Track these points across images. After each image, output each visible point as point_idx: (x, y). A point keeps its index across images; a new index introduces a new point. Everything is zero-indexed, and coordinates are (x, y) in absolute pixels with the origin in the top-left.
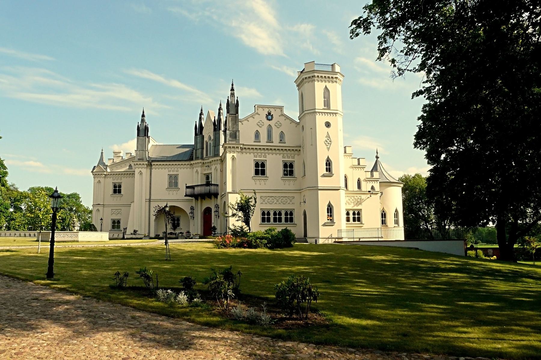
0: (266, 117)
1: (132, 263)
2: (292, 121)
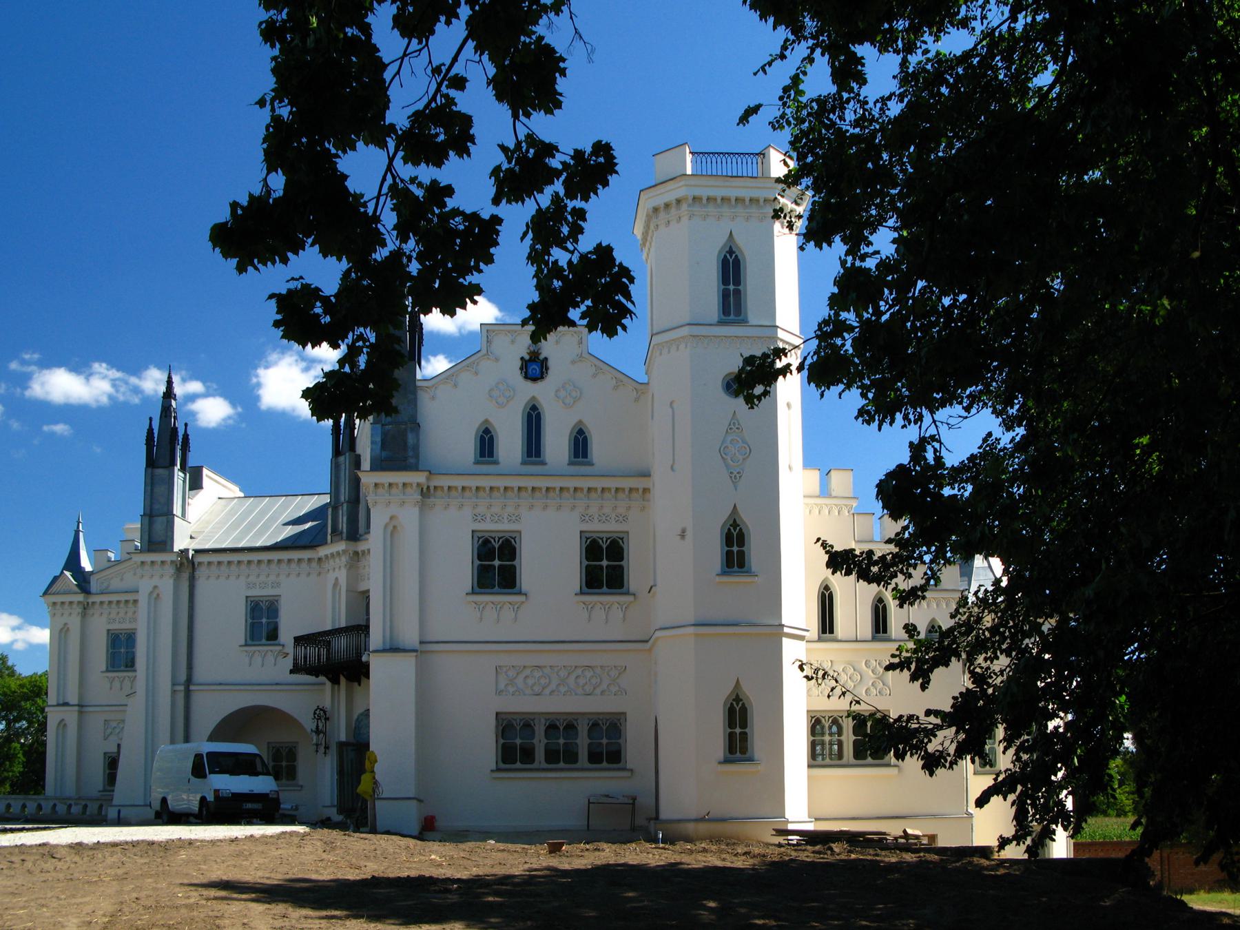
0: (521, 369)
1: (235, 851)
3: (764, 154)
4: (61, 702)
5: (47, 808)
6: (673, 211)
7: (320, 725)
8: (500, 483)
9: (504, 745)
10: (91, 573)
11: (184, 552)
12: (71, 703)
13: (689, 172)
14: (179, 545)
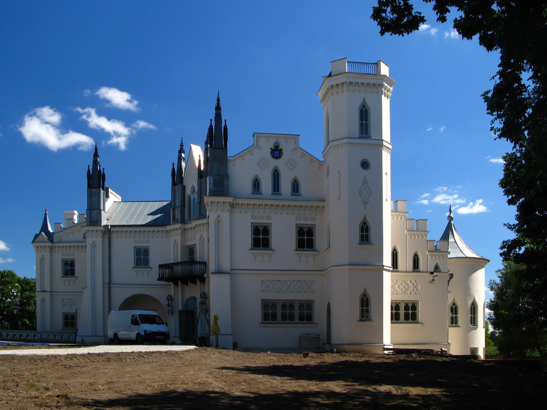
0: (271, 153)
2: (313, 159)
3: (377, 64)
4: (42, 290)
5: (38, 336)
6: (340, 87)
7: (170, 302)
8: (263, 202)
9: (264, 313)
10: (53, 233)
11: (106, 226)
12: (47, 291)
13: (347, 71)
14: (104, 222)
